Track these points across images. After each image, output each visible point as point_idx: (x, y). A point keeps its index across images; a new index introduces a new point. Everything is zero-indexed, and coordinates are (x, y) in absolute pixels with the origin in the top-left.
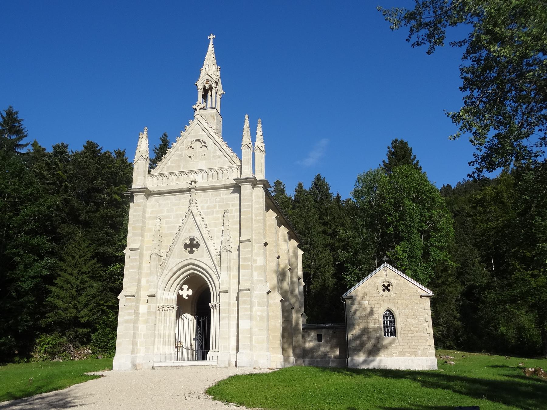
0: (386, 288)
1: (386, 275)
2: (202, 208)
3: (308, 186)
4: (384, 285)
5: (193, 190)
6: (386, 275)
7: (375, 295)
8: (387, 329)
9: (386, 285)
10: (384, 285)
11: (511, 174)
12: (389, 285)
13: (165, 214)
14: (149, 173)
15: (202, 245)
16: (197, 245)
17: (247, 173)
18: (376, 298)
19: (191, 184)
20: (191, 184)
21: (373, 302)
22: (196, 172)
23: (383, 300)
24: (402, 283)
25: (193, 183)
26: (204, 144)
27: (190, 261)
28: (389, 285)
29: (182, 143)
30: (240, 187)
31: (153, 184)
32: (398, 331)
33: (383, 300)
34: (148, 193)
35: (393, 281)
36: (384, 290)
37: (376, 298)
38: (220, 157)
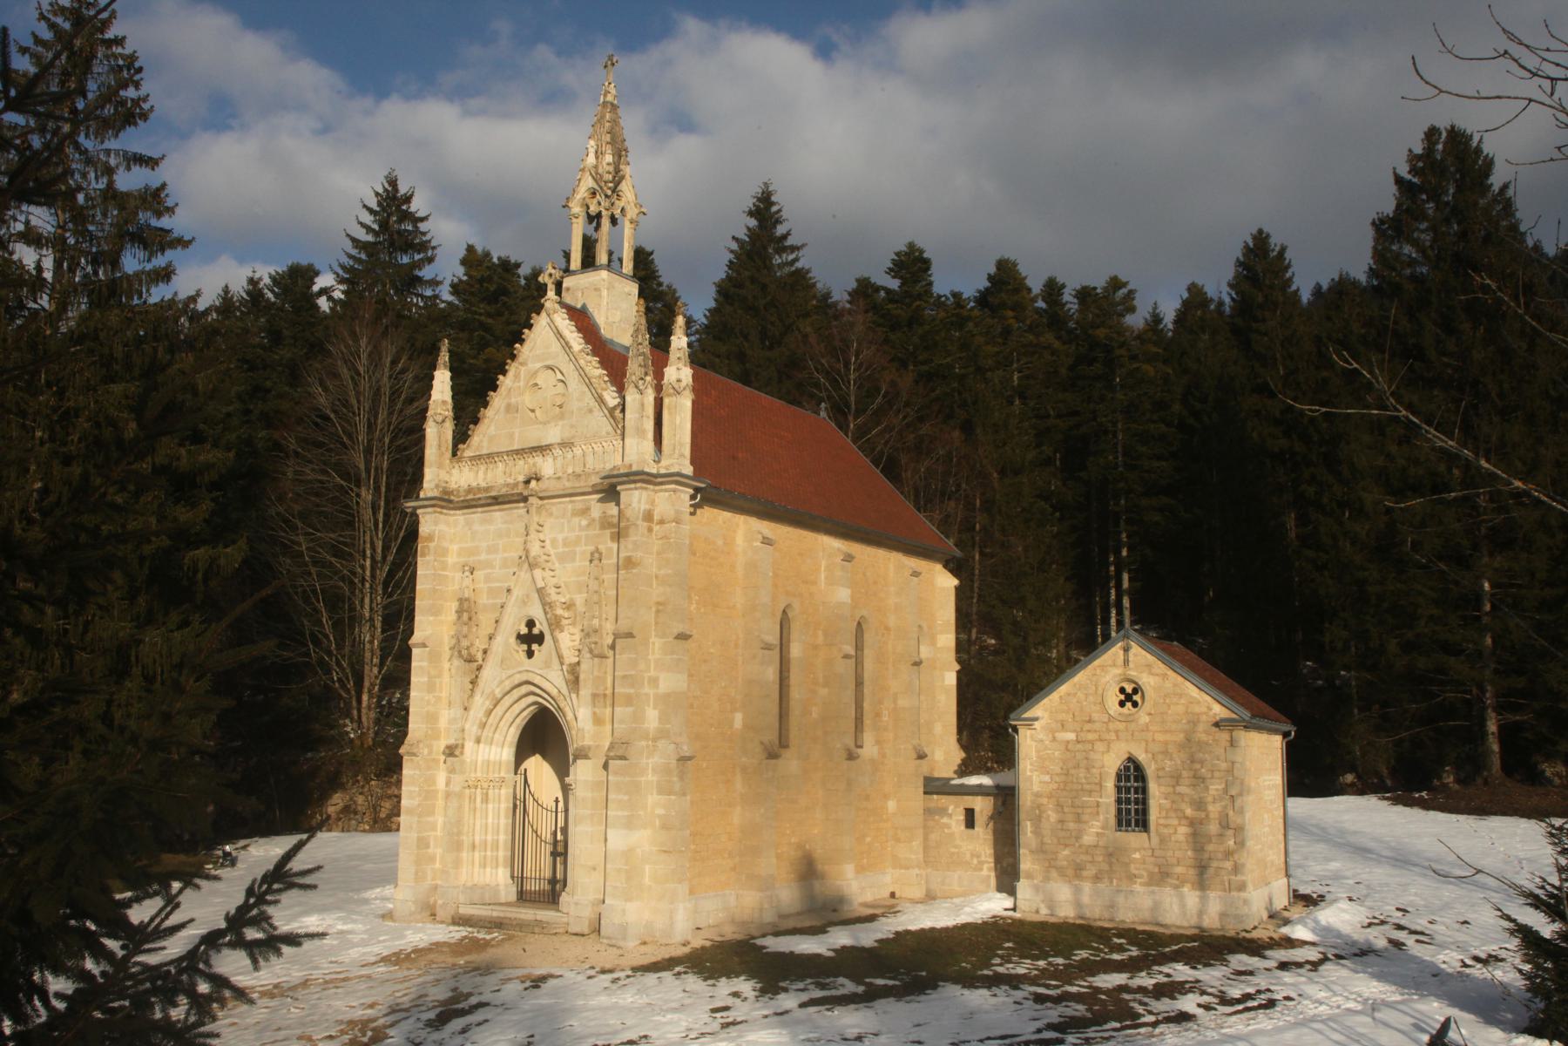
0: (1130, 697)
1: (1126, 662)
2: (554, 541)
3: (1219, 285)
4: (1122, 690)
5: (532, 500)
6: (1126, 662)
7: (1095, 716)
8: (1128, 812)
9: (1129, 690)
10: (1122, 690)
11: (147, 968)
12: (1135, 691)
13: (483, 557)
14: (454, 454)
15: (548, 637)
16: (540, 639)
17: (638, 451)
18: (1097, 726)
19: (527, 482)
20: (527, 482)
21: (1090, 736)
22: (542, 449)
23: (1117, 732)
24: (1168, 684)
25: (533, 483)
26: (560, 376)
27: (524, 677)
28: (1135, 691)
29: (517, 376)
30: (618, 493)
31: (463, 477)
32: (1154, 815)
33: (1117, 732)
34: (446, 501)
35: (1146, 681)
36: (1122, 704)
37: (1097, 726)
38: (591, 411)
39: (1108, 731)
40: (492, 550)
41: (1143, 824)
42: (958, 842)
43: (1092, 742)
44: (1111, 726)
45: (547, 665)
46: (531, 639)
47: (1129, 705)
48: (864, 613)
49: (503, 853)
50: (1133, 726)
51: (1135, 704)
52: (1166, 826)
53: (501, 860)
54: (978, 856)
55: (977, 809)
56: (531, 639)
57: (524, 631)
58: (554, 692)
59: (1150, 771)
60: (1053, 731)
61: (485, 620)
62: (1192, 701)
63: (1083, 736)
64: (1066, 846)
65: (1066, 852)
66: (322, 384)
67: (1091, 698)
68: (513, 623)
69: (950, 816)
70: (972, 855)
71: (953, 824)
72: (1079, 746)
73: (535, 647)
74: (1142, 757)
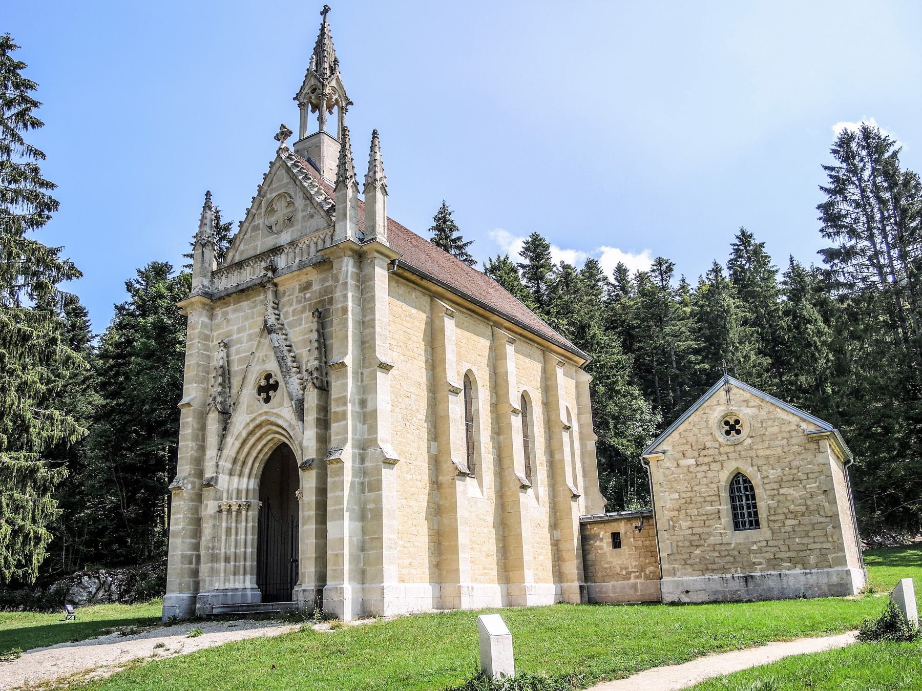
0: (732, 427)
6: (729, 400)
7: (708, 445)
8: (743, 515)
13: (235, 337)
16: (275, 387)
21: (706, 460)
23: (727, 454)
24: (763, 413)
35: (745, 414)
39: (720, 454)
40: (240, 330)
41: (755, 524)
42: (609, 559)
43: (708, 464)
44: (722, 449)
45: (281, 405)
46: (267, 388)
47: (733, 432)
48: (526, 388)
49: (251, 563)
50: (739, 448)
51: (737, 422)
52: (774, 521)
53: (248, 569)
54: (626, 568)
55: (622, 532)
56: (267, 388)
57: (263, 383)
58: (285, 425)
59: (756, 481)
60: (677, 460)
61: (236, 382)
62: (784, 422)
63: (701, 460)
64: (697, 546)
65: (698, 552)
66: (138, 364)
67: (704, 431)
68: (254, 378)
69: (602, 540)
70: (621, 568)
71: (605, 545)
72: (698, 469)
73: (271, 393)
74: (749, 471)
